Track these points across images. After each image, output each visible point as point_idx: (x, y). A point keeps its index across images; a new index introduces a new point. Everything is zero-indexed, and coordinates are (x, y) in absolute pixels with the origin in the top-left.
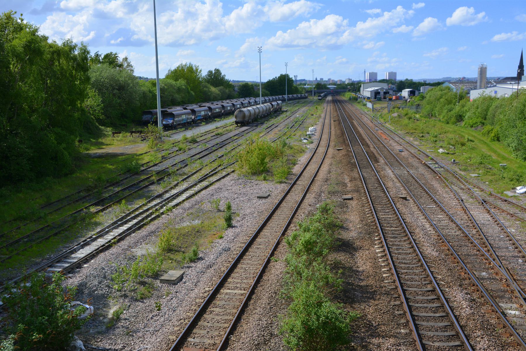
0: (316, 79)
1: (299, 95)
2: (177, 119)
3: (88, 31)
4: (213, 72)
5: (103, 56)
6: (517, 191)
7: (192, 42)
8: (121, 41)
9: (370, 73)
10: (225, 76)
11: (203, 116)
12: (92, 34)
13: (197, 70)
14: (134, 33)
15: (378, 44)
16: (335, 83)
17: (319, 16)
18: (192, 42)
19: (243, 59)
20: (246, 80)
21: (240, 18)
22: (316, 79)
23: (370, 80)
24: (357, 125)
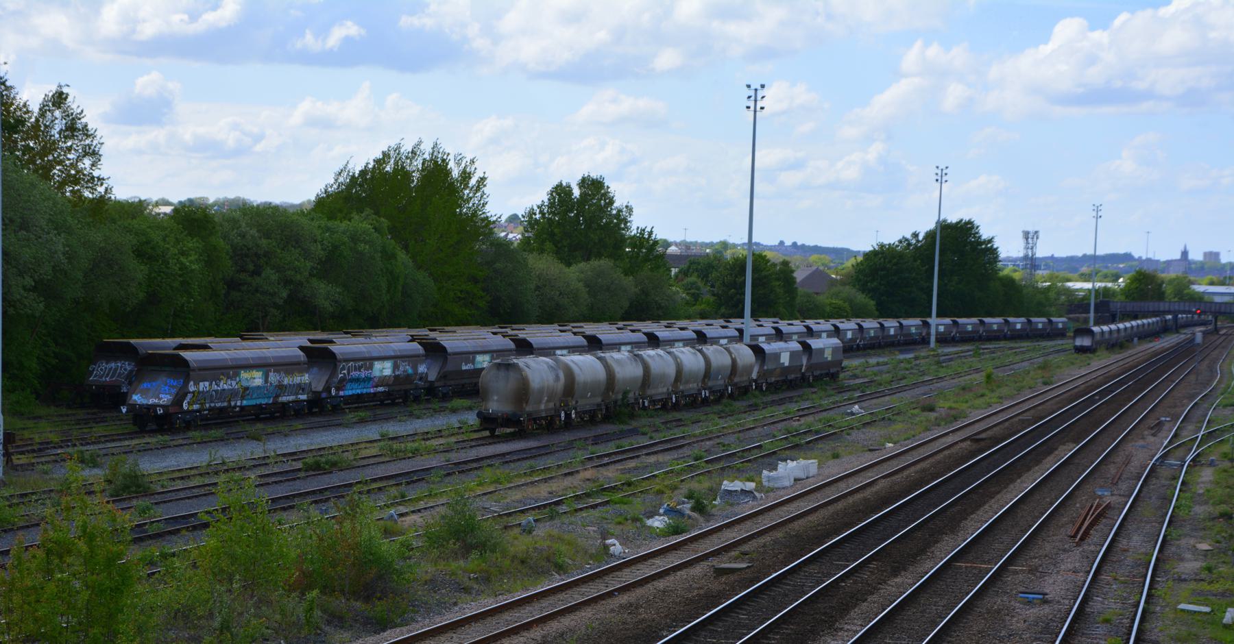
0: (1185, 253)
1: (1019, 323)
2: (204, 386)
4: (576, 192)
7: (667, 59)
8: (347, 40)
10: (630, 209)
11: (382, 381)
13: (466, 176)
18: (667, 59)
19: (875, 151)
20: (1139, 252)
22: (1185, 253)
24: (393, 428)
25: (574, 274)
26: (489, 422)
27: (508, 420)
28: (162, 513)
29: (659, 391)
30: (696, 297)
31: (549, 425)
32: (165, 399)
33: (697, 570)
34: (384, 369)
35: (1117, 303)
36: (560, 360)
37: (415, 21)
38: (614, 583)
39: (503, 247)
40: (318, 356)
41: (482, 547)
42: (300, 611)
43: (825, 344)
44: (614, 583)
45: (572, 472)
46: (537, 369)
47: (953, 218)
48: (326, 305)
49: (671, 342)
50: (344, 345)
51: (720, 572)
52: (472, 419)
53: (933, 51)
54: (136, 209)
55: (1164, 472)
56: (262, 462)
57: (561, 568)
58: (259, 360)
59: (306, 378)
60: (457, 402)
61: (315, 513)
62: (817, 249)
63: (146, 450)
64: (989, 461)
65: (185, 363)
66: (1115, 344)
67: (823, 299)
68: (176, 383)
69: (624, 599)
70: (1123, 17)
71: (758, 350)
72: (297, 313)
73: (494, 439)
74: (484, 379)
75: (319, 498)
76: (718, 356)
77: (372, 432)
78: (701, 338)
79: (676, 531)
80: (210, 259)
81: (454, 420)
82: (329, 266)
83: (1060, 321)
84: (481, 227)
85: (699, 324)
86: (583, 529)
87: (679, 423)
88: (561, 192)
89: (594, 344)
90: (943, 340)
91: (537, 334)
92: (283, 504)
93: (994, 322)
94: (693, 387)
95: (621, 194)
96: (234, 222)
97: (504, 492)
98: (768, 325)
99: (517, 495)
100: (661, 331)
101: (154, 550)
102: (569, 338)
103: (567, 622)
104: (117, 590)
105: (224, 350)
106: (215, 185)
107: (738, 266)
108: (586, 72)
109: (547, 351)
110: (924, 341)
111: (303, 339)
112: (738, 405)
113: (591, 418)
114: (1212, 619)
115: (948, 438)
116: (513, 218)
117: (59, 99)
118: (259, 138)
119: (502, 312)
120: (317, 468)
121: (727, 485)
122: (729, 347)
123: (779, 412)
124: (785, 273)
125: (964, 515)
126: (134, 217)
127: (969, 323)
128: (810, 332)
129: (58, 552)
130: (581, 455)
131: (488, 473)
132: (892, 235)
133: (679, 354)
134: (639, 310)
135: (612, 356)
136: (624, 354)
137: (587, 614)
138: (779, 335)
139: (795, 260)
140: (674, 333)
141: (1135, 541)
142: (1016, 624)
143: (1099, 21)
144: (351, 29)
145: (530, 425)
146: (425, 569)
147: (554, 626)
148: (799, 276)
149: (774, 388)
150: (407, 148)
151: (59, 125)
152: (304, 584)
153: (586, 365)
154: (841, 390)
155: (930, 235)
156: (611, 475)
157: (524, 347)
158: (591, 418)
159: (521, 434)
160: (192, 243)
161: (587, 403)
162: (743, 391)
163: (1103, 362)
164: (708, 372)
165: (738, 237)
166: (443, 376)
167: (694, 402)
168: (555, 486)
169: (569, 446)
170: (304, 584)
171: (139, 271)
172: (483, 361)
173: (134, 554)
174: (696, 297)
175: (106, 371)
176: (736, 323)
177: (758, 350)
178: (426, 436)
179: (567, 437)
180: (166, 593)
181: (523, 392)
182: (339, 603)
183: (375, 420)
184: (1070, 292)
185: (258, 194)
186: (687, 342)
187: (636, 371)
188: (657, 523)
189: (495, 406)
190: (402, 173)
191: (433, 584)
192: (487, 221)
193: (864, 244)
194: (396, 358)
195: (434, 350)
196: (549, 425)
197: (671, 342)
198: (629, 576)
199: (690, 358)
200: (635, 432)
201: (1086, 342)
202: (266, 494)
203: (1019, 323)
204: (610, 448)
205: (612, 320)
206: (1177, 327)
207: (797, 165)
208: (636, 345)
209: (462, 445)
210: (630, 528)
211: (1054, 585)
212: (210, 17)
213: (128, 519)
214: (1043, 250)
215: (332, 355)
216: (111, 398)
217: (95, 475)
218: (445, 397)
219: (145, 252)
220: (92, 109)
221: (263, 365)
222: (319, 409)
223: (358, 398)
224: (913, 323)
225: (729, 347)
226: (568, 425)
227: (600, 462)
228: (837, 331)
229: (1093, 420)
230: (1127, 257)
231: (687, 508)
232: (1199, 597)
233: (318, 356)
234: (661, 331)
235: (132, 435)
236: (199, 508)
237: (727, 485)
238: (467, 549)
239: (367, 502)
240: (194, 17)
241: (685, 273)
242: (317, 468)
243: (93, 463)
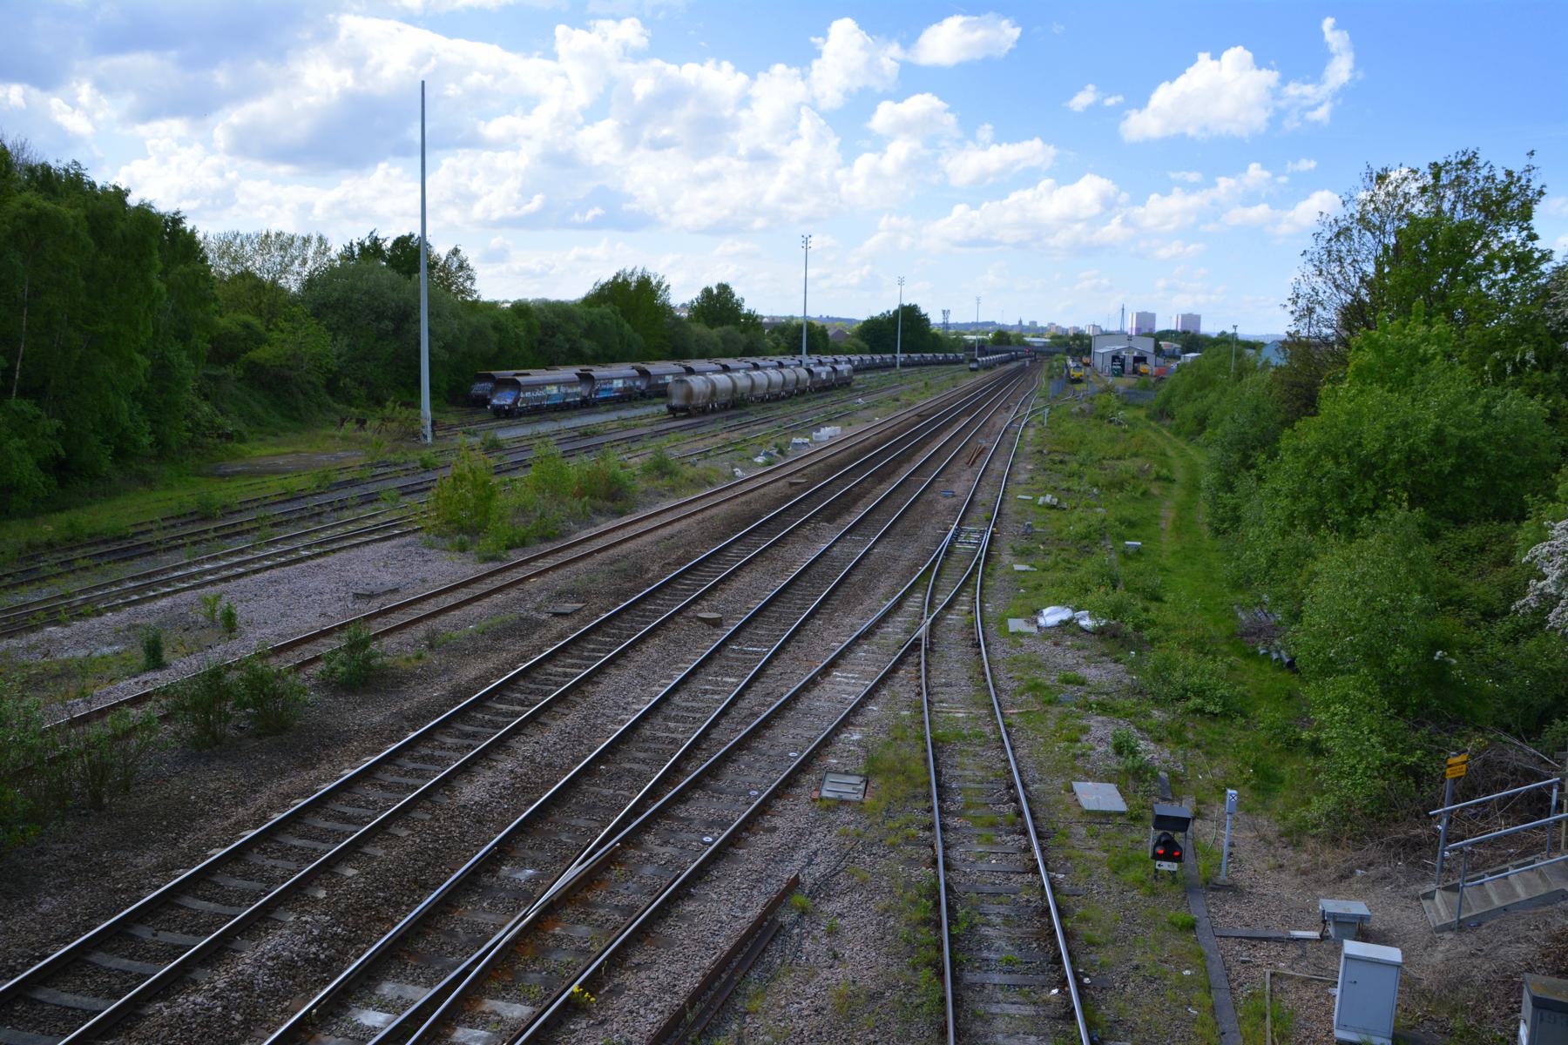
1: (940, 356)
3: (527, 194)
5: (389, 244)
6: (1041, 621)
7: (759, 223)
8: (596, 216)
9: (1138, 315)
11: (618, 390)
12: (537, 202)
13: (659, 284)
14: (631, 198)
15: (1192, 247)
16: (1039, 332)
17: (1065, 175)
18: (759, 223)
20: (999, 321)
21: (875, 175)
23: (1138, 329)
24: (624, 414)
25: (716, 333)
26: (673, 410)
27: (683, 409)
28: (509, 459)
29: (760, 393)
30: (778, 345)
31: (704, 411)
32: (509, 401)
33: (780, 483)
34: (619, 384)
35: (989, 347)
36: (708, 378)
37: (630, 206)
38: (738, 491)
39: (679, 320)
40: (585, 378)
41: (671, 473)
42: (580, 509)
43: (844, 368)
44: (738, 491)
45: (715, 435)
46: (697, 382)
47: (906, 304)
48: (588, 352)
49: (765, 367)
50: (598, 372)
51: (792, 484)
52: (664, 408)
53: (894, 220)
54: (493, 306)
55: (1011, 431)
56: (558, 432)
57: (711, 484)
58: (554, 381)
59: (579, 389)
60: (656, 400)
61: (585, 457)
62: (839, 319)
63: (500, 427)
64: (927, 426)
65: (518, 383)
66: (988, 367)
67: (843, 345)
68: (514, 393)
69: (743, 499)
70: (986, 204)
71: (810, 371)
72: (574, 356)
73: (676, 418)
74: (670, 388)
75: (588, 450)
76: (789, 374)
77: (613, 416)
78: (781, 365)
79: (770, 464)
80: (530, 331)
81: (655, 409)
82: (590, 331)
83: (961, 355)
84: (666, 310)
85: (780, 358)
86: (722, 464)
87: (770, 409)
88: (708, 291)
89: (726, 369)
90: (903, 365)
91: (696, 364)
92: (568, 454)
93: (929, 356)
94: (776, 390)
95: (738, 292)
96: (540, 310)
97: (682, 446)
98: (815, 358)
99: (688, 447)
100: (759, 361)
101: (506, 478)
102: (713, 366)
103: (714, 511)
104: (489, 498)
105: (537, 376)
106: (531, 292)
107: (799, 328)
108: (718, 230)
109: (702, 373)
110: (894, 366)
111: (577, 369)
112: (801, 399)
113: (725, 407)
114: (1033, 503)
115: (904, 414)
116: (683, 305)
117: (456, 252)
118: (552, 268)
119: (678, 353)
120: (586, 435)
121: (795, 440)
122: (795, 370)
123: (821, 402)
124: (823, 332)
125: (914, 454)
126: (1307, 402)
127: (916, 356)
128: (836, 362)
129: (459, 479)
130: (721, 426)
131: (673, 436)
132: (876, 313)
133: (769, 374)
134: (749, 351)
135: (735, 375)
136: (741, 374)
137: (725, 506)
138: (820, 363)
139: (828, 325)
140: (768, 363)
141: (997, 465)
142: (939, 507)
143: (974, 206)
144: (598, 211)
145: (692, 411)
146: (642, 485)
147: (708, 513)
148: (830, 333)
149: (819, 390)
150: (629, 271)
151: (456, 265)
152: (580, 494)
153: (722, 380)
154: (852, 391)
155: (896, 312)
156: (736, 436)
157: (690, 371)
158: (725, 407)
159: (689, 416)
160: (521, 322)
161: (723, 399)
162: (802, 392)
163: (982, 376)
164: (784, 383)
165: (799, 314)
166: (649, 387)
167: (777, 398)
168: (707, 442)
169: (714, 422)
170: (580, 494)
171: (495, 337)
172: (669, 379)
173: (496, 480)
174: (778, 345)
175: (480, 388)
176: (798, 357)
177: (810, 371)
178: (641, 418)
179: (713, 417)
180: (513, 500)
181: (690, 394)
182: (599, 503)
183: (614, 410)
184: (965, 341)
185: (553, 296)
186: (773, 367)
187: (748, 383)
188: (760, 460)
189: (675, 402)
190: (626, 283)
191: (646, 493)
192: (670, 308)
193: (862, 315)
194: (624, 378)
195: (644, 374)
196: (704, 411)
197: (765, 367)
198: (745, 487)
199: (775, 376)
200: (747, 414)
201: (974, 365)
202: (559, 450)
203: (940, 356)
204: (735, 422)
205: (735, 356)
206: (1016, 358)
207: (827, 276)
208: (748, 369)
209: (659, 422)
210: (746, 463)
211: (958, 488)
212: (527, 207)
213: (493, 462)
214: (952, 320)
215: (592, 378)
216: (482, 402)
217: (475, 441)
218: (650, 398)
219: (498, 327)
220: (470, 255)
221: (558, 383)
222: (586, 405)
223: (606, 399)
224: (888, 357)
225: (795, 370)
226: (713, 411)
227: (730, 430)
228: (850, 361)
229: (977, 405)
230: (993, 323)
231: (774, 452)
232: (1027, 492)
233: (585, 378)
234: (760, 362)
235: (493, 420)
236: (528, 456)
237: (795, 440)
238: (663, 475)
239: (612, 451)
240: (518, 207)
241: (772, 332)
242: (586, 435)
243: (475, 435)
